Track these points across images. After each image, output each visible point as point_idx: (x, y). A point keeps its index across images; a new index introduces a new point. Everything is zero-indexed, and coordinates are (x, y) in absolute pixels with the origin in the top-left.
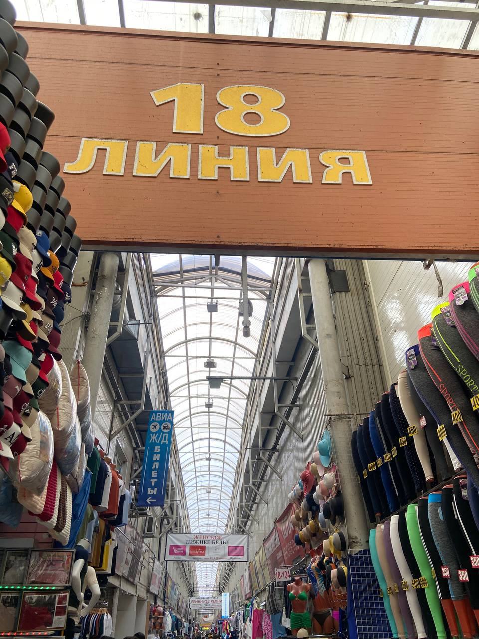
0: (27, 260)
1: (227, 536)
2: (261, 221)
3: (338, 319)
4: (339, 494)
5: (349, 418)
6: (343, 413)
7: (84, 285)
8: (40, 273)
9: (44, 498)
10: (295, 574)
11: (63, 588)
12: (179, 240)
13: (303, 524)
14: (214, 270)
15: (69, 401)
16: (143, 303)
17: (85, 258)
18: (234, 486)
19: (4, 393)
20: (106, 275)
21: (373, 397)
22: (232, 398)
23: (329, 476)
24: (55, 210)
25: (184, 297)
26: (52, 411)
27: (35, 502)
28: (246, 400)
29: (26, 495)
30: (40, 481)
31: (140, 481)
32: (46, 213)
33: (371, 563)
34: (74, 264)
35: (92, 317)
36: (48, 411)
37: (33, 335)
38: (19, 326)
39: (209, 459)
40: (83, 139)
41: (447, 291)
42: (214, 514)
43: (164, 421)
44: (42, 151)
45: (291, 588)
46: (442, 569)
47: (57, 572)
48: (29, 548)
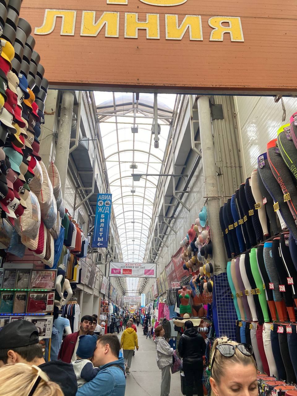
1: (144, 265)
2: (167, 68)
3: (215, 138)
4: (210, 242)
5: (219, 199)
6: (215, 196)
7: (53, 114)
8: (23, 103)
9: (37, 241)
10: (183, 285)
11: (51, 290)
12: (112, 82)
13: (188, 259)
14: (136, 105)
15: (48, 186)
16: (91, 126)
17: (52, 95)
18: (148, 238)
19: (7, 179)
20: (66, 107)
21: (234, 186)
22: (147, 187)
23: (205, 232)
24: (30, 60)
25: (116, 123)
26: (38, 191)
27: (32, 243)
28: (156, 189)
29: (26, 239)
30: (34, 231)
31: (94, 235)
32: (24, 62)
33: (227, 280)
34: (45, 98)
35: (59, 135)
36: (35, 191)
37: (22, 144)
38: (12, 138)
39: (133, 222)
40: (47, 10)
41: (288, 117)
42: (136, 252)
43: (106, 200)
45: (180, 292)
46: (270, 284)
47: (47, 282)
48: (30, 269)
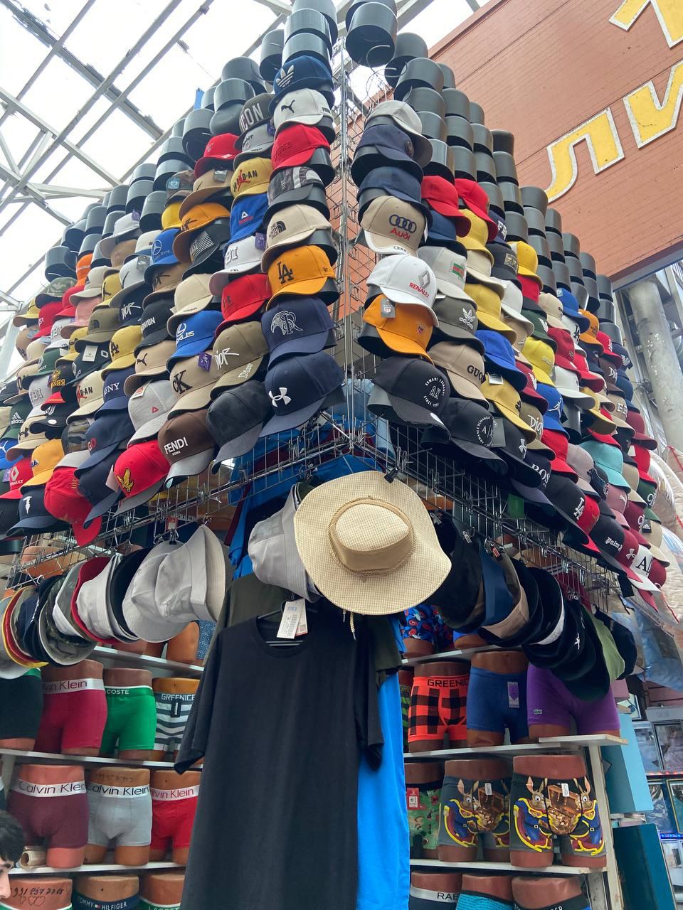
0: (562, 332)
20: (646, 316)
26: (671, 522)
35: (654, 383)
38: (589, 419)
40: (549, 148)
44: (519, 187)
